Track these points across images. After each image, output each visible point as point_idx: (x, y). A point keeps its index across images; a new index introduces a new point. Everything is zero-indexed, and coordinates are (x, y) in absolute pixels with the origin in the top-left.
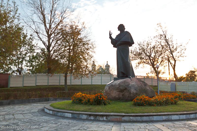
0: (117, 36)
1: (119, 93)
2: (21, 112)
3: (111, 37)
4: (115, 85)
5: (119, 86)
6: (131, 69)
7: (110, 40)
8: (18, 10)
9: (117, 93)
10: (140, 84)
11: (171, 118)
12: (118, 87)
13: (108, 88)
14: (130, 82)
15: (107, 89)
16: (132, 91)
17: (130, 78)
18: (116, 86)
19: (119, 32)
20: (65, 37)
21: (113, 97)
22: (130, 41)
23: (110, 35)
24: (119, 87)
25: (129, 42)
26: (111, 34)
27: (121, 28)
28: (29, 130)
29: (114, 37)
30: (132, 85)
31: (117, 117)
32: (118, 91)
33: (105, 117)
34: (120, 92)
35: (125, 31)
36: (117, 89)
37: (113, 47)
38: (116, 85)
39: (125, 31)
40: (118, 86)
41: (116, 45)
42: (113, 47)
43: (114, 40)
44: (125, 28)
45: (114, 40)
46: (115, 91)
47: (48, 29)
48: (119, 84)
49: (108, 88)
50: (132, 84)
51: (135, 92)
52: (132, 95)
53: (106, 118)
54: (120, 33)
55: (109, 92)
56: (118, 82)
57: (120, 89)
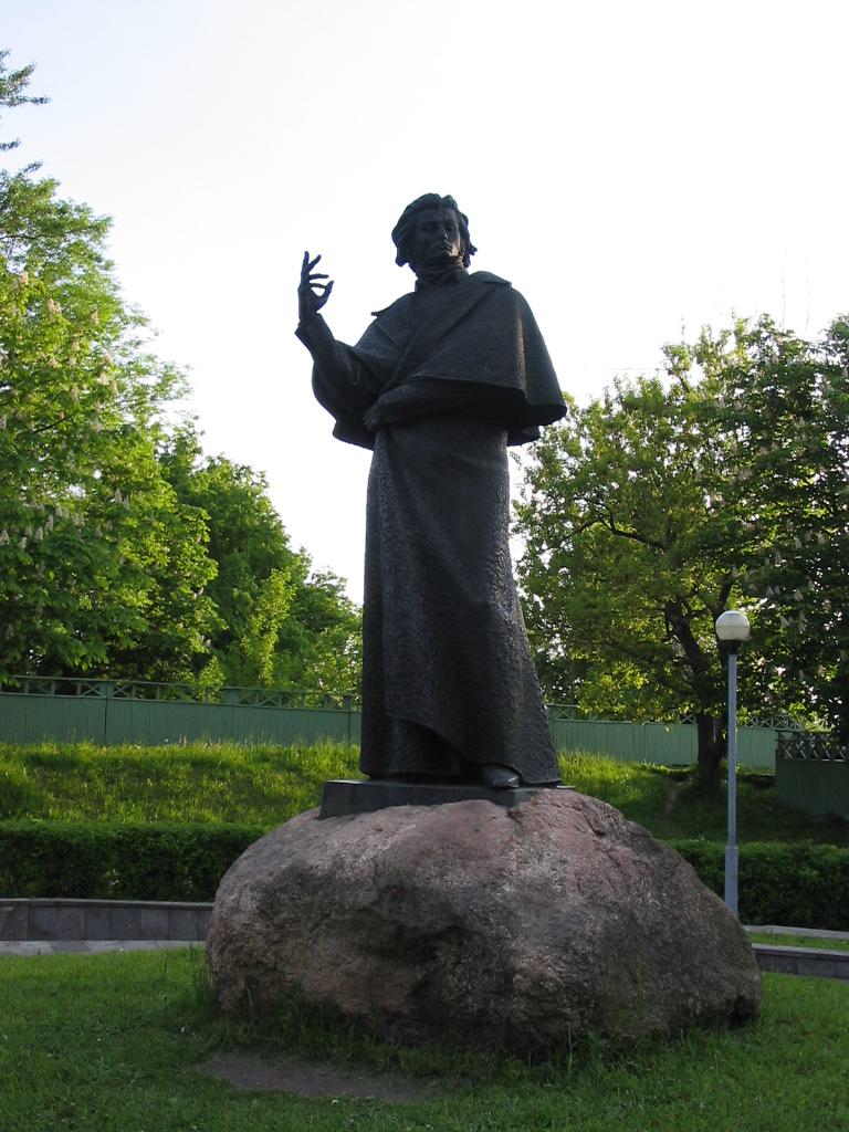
0: (386, 320)
1: (372, 962)
3: (312, 330)
4: (332, 873)
6: (403, 228)
7: (304, 361)
8: (693, 340)
10: (614, 875)
12: (364, 898)
13: (249, 903)
14: (506, 847)
17: (502, 795)
18: (348, 886)
19: (404, 281)
22: (523, 386)
23: (310, 303)
25: (521, 392)
26: (319, 292)
27: (373, 314)
29: (348, 323)
30: (522, 885)
32: (364, 949)
34: (385, 953)
35: (407, 264)
36: (356, 926)
38: (339, 874)
39: (471, 270)
40: (374, 895)
41: (371, 419)
43: (348, 363)
44: (474, 241)
45: (348, 363)
46: (328, 946)
47: (310, 261)
50: (528, 872)
51: (554, 971)
52: (519, 1007)
54: (412, 289)
55: (261, 943)
56: (372, 839)
57: (391, 929)
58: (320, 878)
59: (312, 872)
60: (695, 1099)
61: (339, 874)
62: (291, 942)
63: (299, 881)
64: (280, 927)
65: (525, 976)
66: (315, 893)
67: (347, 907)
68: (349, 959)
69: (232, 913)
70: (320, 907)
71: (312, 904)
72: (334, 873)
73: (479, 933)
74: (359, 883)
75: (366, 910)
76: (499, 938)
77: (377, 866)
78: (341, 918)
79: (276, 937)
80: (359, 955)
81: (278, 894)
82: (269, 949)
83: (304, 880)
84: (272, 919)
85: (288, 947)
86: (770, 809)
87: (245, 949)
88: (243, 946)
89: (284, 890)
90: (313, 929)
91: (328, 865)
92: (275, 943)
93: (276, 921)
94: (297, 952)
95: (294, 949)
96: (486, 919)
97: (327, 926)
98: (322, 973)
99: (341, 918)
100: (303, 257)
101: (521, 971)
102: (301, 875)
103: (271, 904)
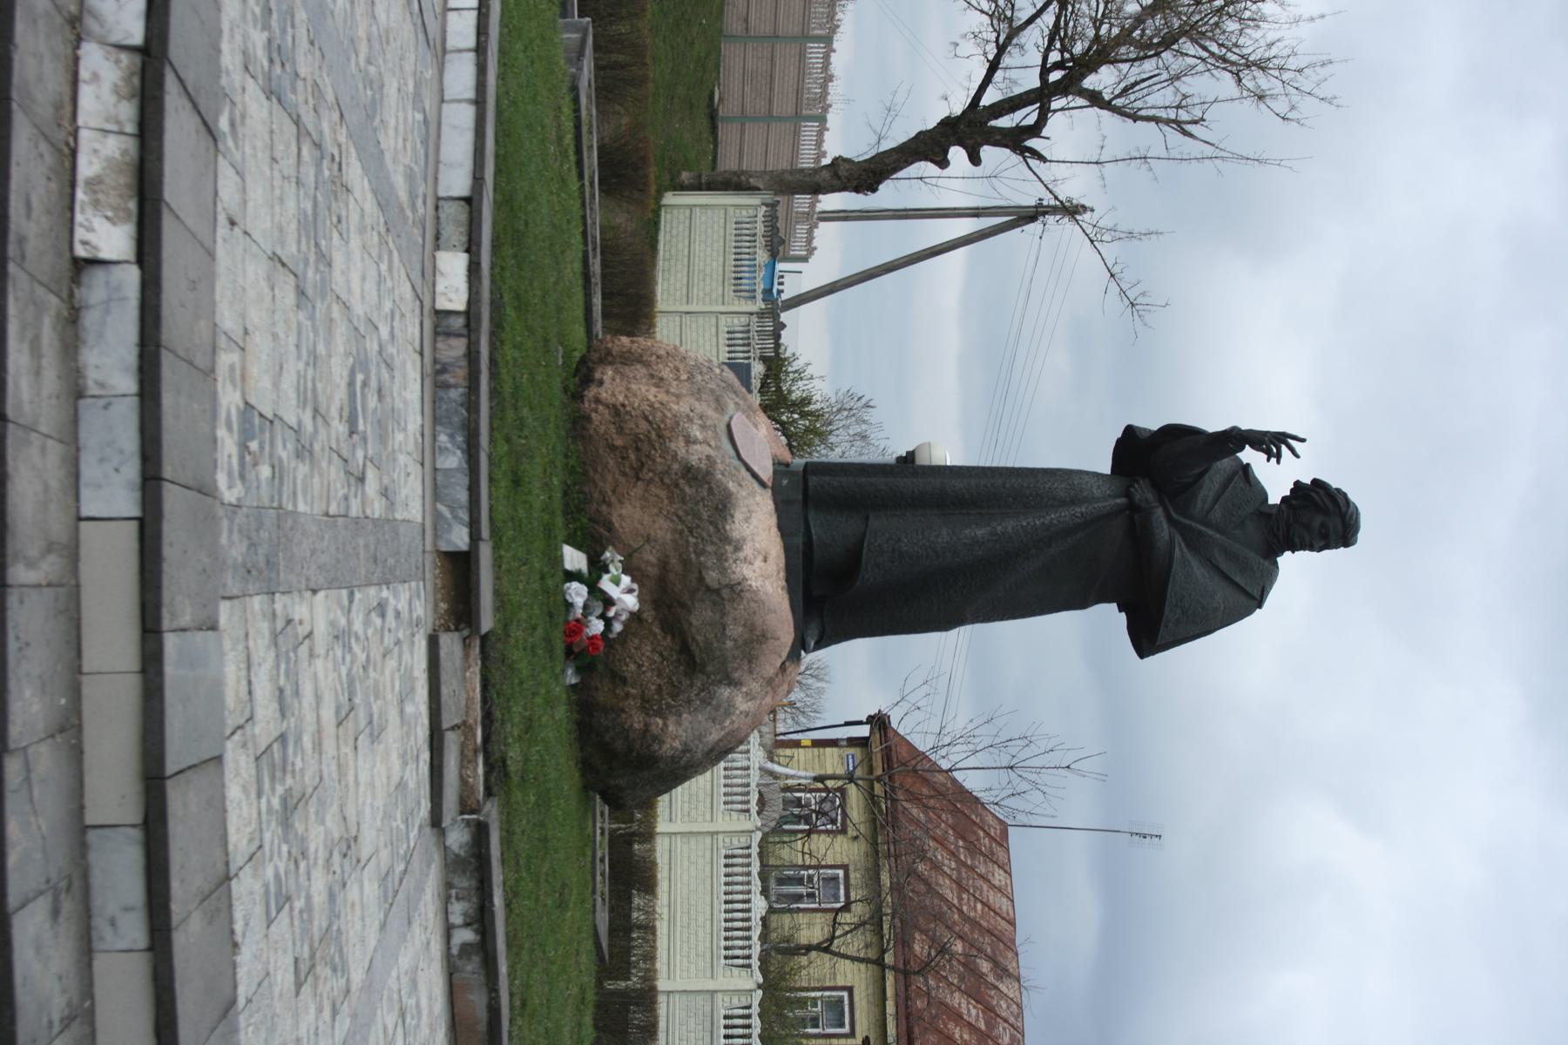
2: (566, 166)
5: (717, 592)
9: (653, 559)
11: (267, 479)
12: (712, 577)
15: (682, 452)
16: (671, 728)
18: (721, 558)
20: (1134, 35)
21: (609, 505)
24: (708, 589)
28: (469, 700)
31: (445, 806)
32: (664, 564)
33: (478, 938)
35: (1247, 446)
37: (1130, 431)
38: (729, 548)
42: (1130, 431)
48: (736, 590)
49: (694, 460)
53: (466, 949)
58: (724, 528)
59: (728, 517)
60: (503, 553)
61: (729, 548)
62: (663, 494)
63: (720, 506)
64: (677, 485)
65: (662, 729)
66: (711, 523)
67: (702, 559)
68: (654, 551)
69: (684, 436)
70: (698, 526)
71: (700, 519)
72: (730, 544)
73: (691, 686)
74: (723, 571)
75: (701, 579)
76: (689, 702)
77: (739, 584)
78: (691, 549)
79: (667, 481)
80: (659, 560)
81: (706, 486)
82: (655, 474)
83: (721, 510)
84: (683, 478)
85: (658, 491)
86: (640, 145)
87: (653, 452)
88: (655, 449)
89: (710, 489)
90: (677, 516)
91: (735, 535)
92: (662, 480)
93: (682, 482)
94: (656, 499)
95: (658, 496)
96: (703, 690)
97: (681, 533)
98: (639, 527)
99: (691, 549)
100: (1301, 436)
101: (665, 724)
102: (725, 506)
103: (697, 479)
